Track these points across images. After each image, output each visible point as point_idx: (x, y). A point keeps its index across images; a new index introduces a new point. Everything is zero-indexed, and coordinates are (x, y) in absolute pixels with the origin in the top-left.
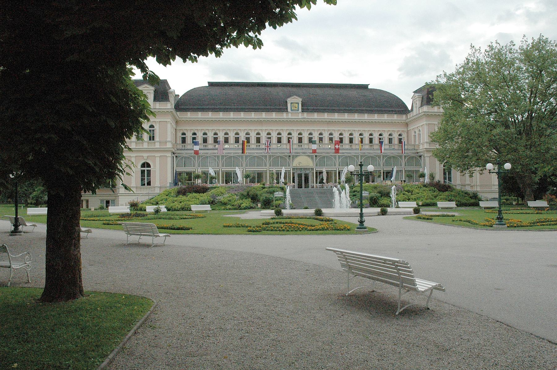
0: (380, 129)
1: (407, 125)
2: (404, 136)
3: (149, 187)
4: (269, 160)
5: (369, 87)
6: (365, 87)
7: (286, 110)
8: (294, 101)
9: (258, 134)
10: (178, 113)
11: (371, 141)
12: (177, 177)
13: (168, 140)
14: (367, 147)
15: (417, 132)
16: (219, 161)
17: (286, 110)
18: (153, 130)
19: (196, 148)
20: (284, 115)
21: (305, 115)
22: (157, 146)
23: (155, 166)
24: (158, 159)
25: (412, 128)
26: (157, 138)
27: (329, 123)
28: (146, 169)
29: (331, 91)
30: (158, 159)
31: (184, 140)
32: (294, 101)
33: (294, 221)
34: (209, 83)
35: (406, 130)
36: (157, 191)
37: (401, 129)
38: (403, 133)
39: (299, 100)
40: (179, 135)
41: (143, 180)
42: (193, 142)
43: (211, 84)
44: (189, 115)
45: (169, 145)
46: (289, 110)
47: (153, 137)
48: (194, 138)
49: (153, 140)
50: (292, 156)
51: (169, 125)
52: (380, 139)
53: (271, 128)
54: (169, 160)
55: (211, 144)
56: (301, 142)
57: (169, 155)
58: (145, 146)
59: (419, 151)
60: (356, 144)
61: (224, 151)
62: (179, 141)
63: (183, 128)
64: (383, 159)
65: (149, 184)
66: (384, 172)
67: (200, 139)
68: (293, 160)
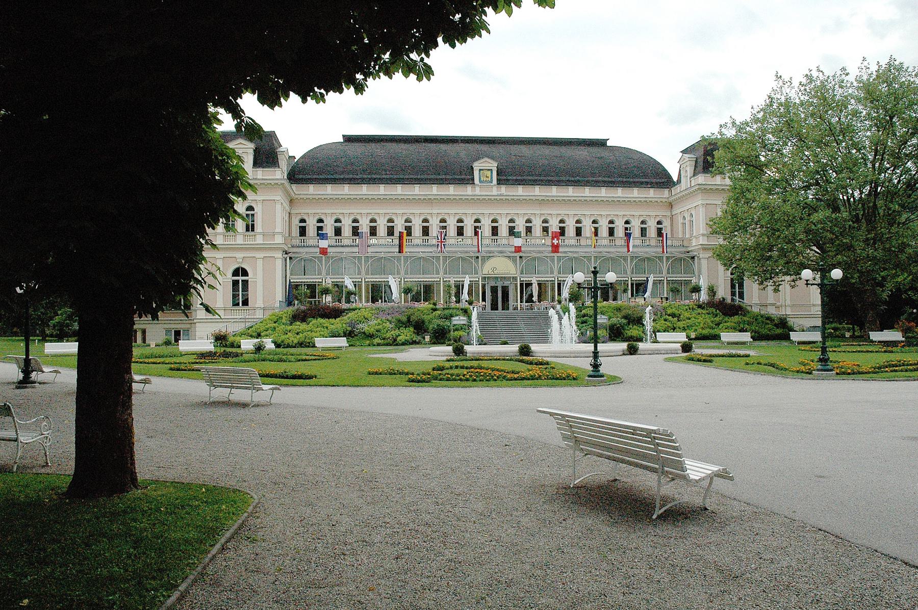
0: (627, 212)
1: (671, 206)
2: (666, 224)
3: (245, 307)
4: (444, 263)
5: (609, 143)
6: (601, 143)
7: (471, 181)
8: (485, 167)
9: (355, 221)
10: (294, 186)
11: (611, 232)
12: (292, 292)
13: (277, 230)
14: (605, 242)
15: (688, 218)
16: (361, 264)
17: (471, 181)
18: (253, 215)
19: (324, 244)
20: (468, 190)
21: (503, 189)
22: (259, 240)
23: (255, 274)
24: (260, 263)
25: (679, 211)
26: (258, 228)
27: (542, 202)
28: (240, 278)
29: (546, 150)
30: (260, 263)
31: (303, 231)
32: (485, 167)
33: (484, 364)
34: (344, 136)
35: (669, 214)
36: (259, 315)
37: (661, 213)
38: (663, 220)
39: (494, 165)
40: (296, 223)
41: (235, 296)
42: (318, 235)
43: (348, 139)
44: (311, 190)
45: (279, 240)
46: (477, 181)
47: (253, 225)
48: (320, 228)
49: (253, 230)
50: (479, 258)
51: (278, 206)
52: (626, 229)
53: (464, 211)
54: (279, 264)
55: (347, 238)
56: (497, 235)
57: (279, 255)
58: (240, 240)
59: (690, 249)
60: (587, 238)
61: (370, 250)
62: (296, 232)
63: (302, 211)
64: (631, 262)
65: (246, 303)
66: (632, 284)
67: (329, 230)
68: (482, 264)
